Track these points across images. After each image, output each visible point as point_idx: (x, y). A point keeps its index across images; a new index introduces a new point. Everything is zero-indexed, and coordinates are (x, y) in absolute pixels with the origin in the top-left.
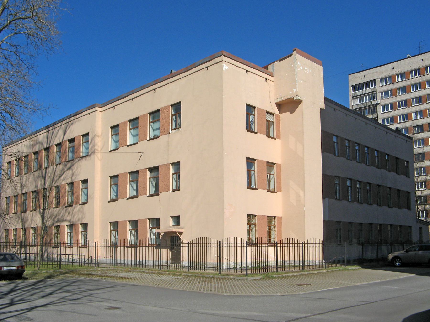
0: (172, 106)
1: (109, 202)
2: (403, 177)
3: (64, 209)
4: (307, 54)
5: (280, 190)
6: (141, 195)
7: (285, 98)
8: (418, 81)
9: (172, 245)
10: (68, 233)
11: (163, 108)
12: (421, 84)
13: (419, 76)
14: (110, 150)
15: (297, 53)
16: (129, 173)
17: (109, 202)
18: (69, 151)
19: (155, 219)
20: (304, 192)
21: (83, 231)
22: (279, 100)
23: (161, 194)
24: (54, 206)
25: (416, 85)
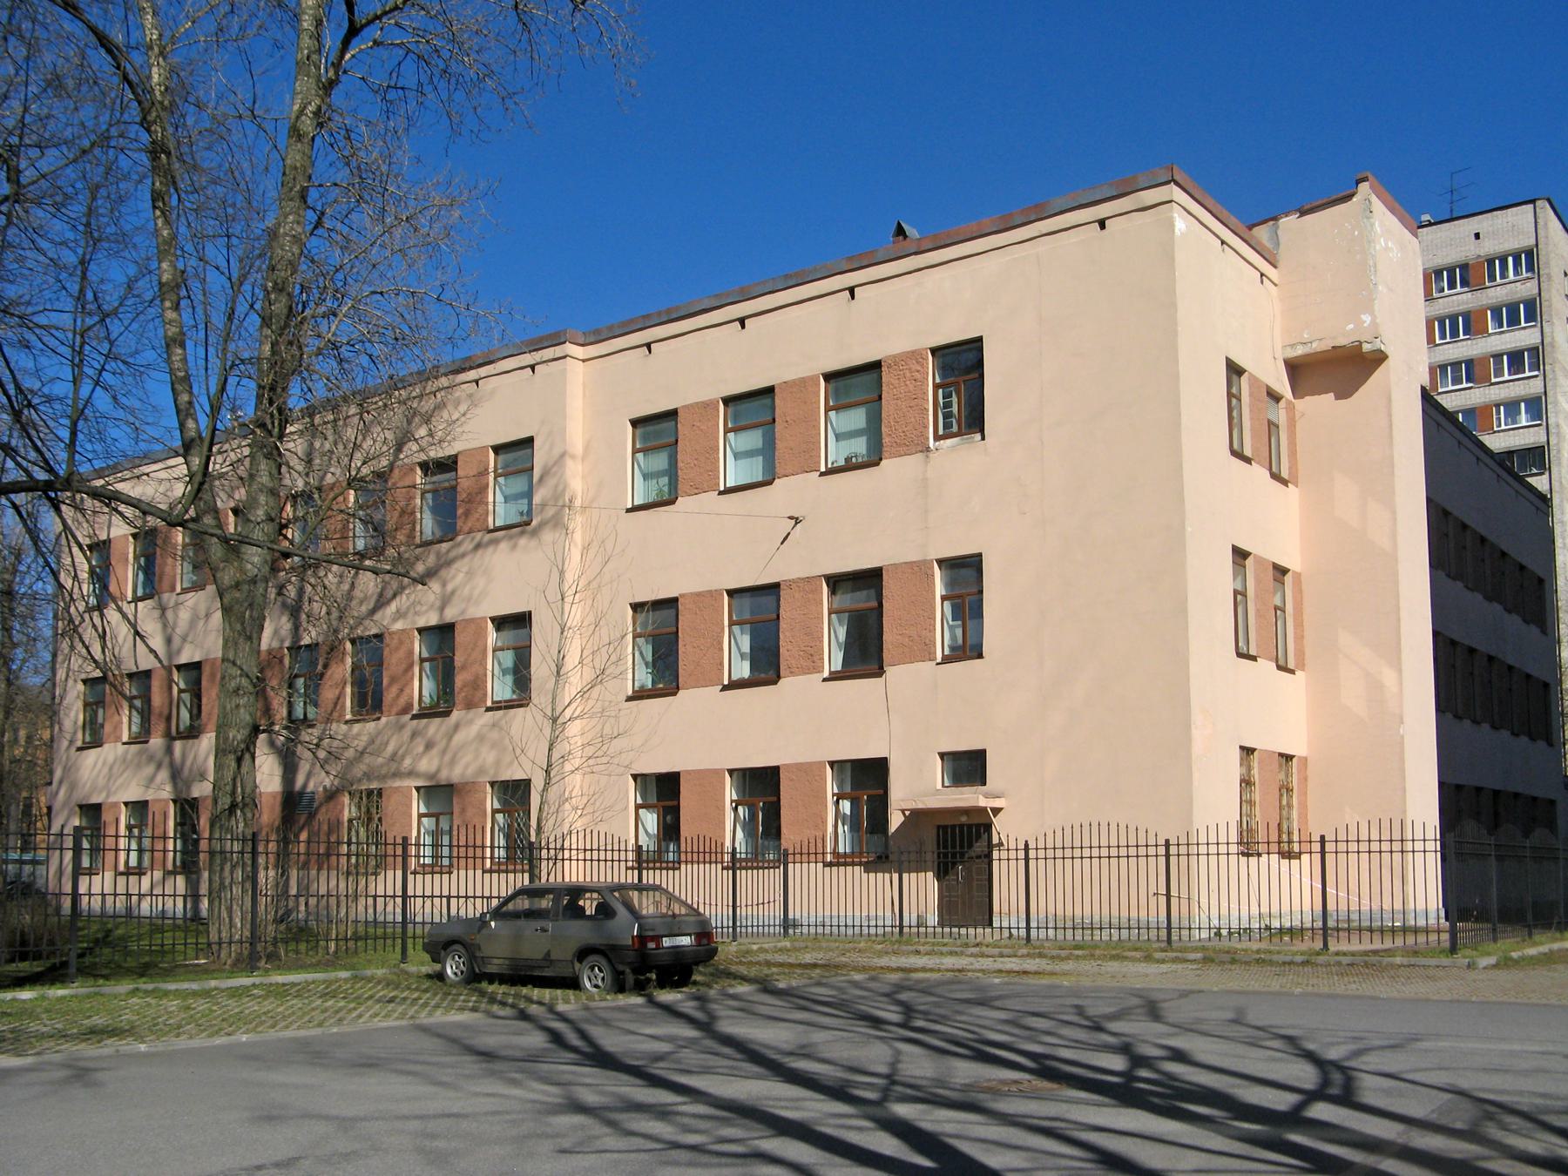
0: (934, 351)
1: (629, 699)
2: (1534, 630)
3: (402, 727)
4: (1389, 197)
5: (1301, 665)
6: (792, 674)
7: (1326, 345)
8: (1462, 308)
9: (946, 855)
10: (420, 816)
11: (894, 356)
12: (1473, 318)
13: (1466, 289)
14: (630, 506)
15: (1371, 187)
16: (731, 593)
17: (629, 699)
18: (425, 508)
19: (849, 765)
20: (1400, 671)
21: (498, 811)
22: (1300, 351)
23: (891, 671)
24: (349, 717)
25: (1453, 319)
